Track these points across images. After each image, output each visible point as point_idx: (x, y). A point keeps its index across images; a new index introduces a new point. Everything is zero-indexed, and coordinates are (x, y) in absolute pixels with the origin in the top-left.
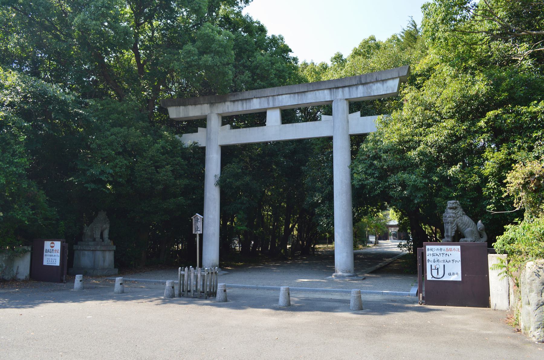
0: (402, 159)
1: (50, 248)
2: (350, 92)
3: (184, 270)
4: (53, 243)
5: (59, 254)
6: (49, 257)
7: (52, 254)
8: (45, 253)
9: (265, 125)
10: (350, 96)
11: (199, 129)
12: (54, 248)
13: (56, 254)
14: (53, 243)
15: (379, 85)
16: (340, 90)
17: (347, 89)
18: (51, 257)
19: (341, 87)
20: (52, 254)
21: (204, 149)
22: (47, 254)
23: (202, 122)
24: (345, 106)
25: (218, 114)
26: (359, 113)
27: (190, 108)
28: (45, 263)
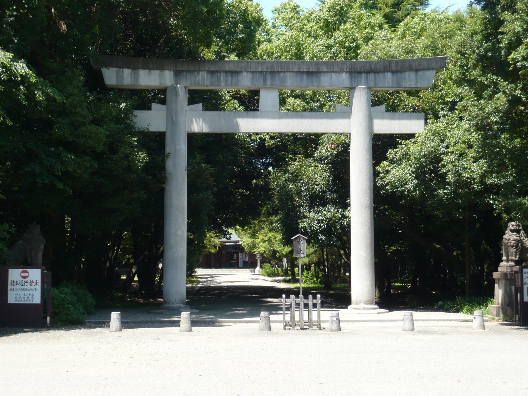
0: (154, 158)
1: (22, 279)
2: (375, 79)
3: (307, 298)
4: (27, 272)
5: (39, 287)
6: (19, 292)
7: (25, 287)
8: (10, 287)
9: (258, 110)
10: (417, 83)
11: (154, 105)
12: (28, 279)
13: (33, 287)
14: (27, 272)
15: (412, 74)
16: (364, 75)
17: (372, 76)
18: (23, 292)
19: (364, 72)
20: (25, 287)
21: (162, 136)
22: (15, 287)
23: (160, 96)
24: (183, 96)
25: (185, 87)
26: (200, 105)
27: (143, 73)
28: (12, 299)
